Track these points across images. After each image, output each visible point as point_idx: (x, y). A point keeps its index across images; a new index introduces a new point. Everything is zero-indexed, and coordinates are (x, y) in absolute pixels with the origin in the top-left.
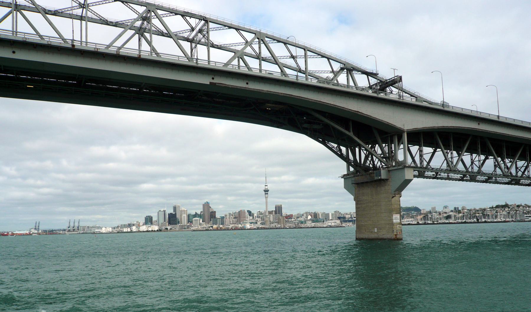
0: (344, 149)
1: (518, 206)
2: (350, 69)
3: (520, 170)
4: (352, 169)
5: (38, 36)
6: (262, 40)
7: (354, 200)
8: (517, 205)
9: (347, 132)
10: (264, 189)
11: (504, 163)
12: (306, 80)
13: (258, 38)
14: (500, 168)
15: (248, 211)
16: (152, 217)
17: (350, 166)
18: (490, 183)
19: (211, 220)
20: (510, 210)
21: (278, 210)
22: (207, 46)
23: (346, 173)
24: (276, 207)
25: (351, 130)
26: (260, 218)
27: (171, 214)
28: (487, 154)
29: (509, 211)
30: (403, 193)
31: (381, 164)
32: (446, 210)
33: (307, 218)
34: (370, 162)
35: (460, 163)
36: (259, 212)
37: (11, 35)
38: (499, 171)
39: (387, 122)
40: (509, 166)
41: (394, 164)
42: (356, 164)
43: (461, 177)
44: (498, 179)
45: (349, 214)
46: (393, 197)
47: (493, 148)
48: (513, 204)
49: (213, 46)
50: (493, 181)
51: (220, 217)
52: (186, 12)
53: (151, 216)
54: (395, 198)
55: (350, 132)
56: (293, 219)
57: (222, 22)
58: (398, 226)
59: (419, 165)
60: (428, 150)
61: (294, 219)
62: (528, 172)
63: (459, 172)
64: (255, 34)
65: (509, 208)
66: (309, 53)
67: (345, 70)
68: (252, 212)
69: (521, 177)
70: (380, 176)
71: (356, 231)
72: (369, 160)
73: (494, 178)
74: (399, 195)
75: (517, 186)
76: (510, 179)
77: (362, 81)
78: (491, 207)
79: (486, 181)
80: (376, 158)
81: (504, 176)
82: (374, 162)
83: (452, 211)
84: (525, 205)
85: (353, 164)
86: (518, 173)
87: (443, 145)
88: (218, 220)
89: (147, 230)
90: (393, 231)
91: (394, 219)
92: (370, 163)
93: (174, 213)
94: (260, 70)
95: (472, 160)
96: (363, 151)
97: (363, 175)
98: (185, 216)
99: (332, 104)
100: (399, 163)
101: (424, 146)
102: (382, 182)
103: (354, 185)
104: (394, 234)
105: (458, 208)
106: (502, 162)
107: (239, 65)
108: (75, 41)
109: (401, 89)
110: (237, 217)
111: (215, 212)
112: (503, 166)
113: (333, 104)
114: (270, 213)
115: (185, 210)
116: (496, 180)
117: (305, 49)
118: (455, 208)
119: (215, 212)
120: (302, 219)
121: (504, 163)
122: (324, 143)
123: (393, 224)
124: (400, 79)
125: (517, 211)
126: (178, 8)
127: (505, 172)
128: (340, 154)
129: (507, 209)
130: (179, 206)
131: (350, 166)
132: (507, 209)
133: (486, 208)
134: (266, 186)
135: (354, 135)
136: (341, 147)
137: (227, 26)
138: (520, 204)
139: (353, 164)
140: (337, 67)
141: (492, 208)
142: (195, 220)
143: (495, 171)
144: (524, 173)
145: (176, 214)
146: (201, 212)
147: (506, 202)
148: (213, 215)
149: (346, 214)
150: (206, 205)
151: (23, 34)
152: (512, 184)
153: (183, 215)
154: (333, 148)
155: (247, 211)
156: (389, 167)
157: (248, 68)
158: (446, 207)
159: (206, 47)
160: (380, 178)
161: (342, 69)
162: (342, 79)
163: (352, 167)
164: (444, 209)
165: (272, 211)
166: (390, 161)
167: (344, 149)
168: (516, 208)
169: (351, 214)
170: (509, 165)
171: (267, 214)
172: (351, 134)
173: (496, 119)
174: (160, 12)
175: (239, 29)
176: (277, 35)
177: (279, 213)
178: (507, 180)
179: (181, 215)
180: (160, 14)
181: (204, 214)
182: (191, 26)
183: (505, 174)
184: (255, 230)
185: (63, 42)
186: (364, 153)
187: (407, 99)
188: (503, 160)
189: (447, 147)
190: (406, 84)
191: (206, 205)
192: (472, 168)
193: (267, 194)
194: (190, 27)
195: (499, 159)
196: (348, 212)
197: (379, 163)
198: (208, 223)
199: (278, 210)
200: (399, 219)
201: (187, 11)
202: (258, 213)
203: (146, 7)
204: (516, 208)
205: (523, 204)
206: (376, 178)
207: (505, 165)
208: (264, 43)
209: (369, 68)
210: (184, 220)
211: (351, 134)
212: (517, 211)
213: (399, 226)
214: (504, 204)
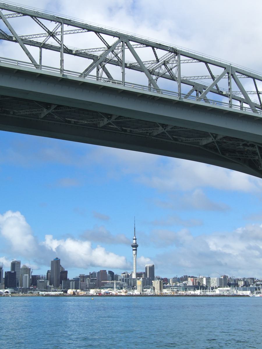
5: (33, 65)
12: (241, 109)
19: (61, 283)
22: (121, 66)
49: (69, 52)
52: (158, 44)
57: (193, 54)
64: (225, 68)
88: (71, 283)
93: (13, 272)
94: (241, 107)
107: (97, 76)
108: (65, 70)
110: (96, 279)
119: (66, 272)
126: (120, 31)
137: (197, 59)
145: (15, 273)
151: (17, 62)
155: (109, 271)
157: (35, 65)
159: (120, 67)
169: (245, 280)
174: (131, 43)
175: (35, 17)
180: (131, 45)
182: (107, 45)
185: (35, 68)
194: (106, 45)
201: (159, 43)
203: (118, 38)
208: (233, 77)
210: (26, 281)
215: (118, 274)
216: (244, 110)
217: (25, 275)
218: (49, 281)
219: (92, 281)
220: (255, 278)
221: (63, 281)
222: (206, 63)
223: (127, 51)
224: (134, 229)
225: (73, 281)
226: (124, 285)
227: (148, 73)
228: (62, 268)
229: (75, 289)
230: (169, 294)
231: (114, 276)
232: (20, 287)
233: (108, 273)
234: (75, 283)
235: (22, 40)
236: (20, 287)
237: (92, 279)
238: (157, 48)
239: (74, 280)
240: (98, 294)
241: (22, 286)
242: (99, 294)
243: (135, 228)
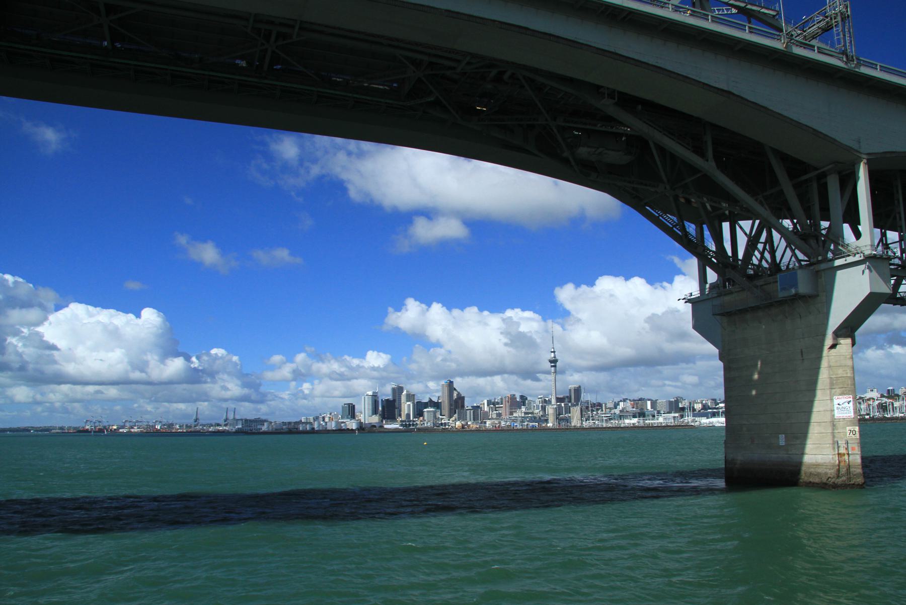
0: (691, 228)
7: (721, 359)
16: (354, 406)
17: (707, 268)
23: (696, 293)
27: (387, 400)
31: (794, 255)
34: (762, 254)
39: (815, 128)
53: (352, 404)
55: (707, 161)
58: (848, 428)
70: (795, 285)
71: (726, 443)
72: (759, 251)
80: (779, 236)
82: (773, 252)
85: (715, 261)
88: (468, 412)
89: (340, 428)
92: (762, 257)
97: (743, 290)
98: (410, 405)
99: (650, 63)
103: (718, 317)
110: (502, 407)
113: (657, 64)
128: (680, 233)
131: (707, 268)
135: (718, 168)
136: (687, 224)
139: (715, 261)
142: (428, 411)
154: (660, 218)
160: (793, 291)
163: (711, 268)
166: (819, 246)
167: (691, 228)
172: (709, 166)
184: (280, 436)
186: (746, 234)
197: (789, 253)
206: (782, 295)
211: (709, 166)
213: (851, 428)
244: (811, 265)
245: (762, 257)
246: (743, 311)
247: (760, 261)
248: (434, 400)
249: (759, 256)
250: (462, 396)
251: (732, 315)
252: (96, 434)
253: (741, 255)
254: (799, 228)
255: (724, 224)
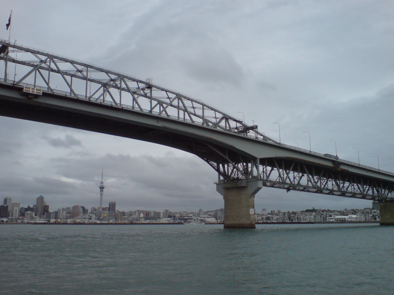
1: (323, 211)
2: (226, 118)
3: (322, 184)
4: (222, 178)
6: (180, 99)
8: (322, 210)
9: (224, 156)
10: (100, 186)
11: (313, 179)
13: (178, 98)
14: (311, 182)
15: (81, 207)
18: (305, 191)
19: (44, 214)
20: (317, 214)
21: (112, 206)
23: (218, 182)
24: (110, 204)
25: (227, 156)
26: (94, 214)
28: (303, 172)
29: (316, 215)
30: (256, 195)
32: (265, 213)
33: (140, 215)
34: (235, 174)
35: (288, 179)
36: (93, 208)
37: (46, 91)
38: (310, 184)
40: (316, 181)
41: (250, 177)
42: (224, 174)
43: (288, 187)
44: (309, 189)
45: (179, 214)
46: (250, 198)
47: (307, 169)
48: (319, 209)
50: (307, 190)
51: (54, 211)
54: (251, 198)
56: (126, 216)
59: (262, 179)
60: (269, 168)
61: (127, 216)
62: (327, 185)
63: (287, 184)
65: (316, 212)
66: (205, 107)
67: (224, 119)
68: (85, 208)
69: (323, 188)
73: (307, 189)
74: (253, 197)
75: (321, 194)
76: (317, 189)
77: (233, 124)
78: (302, 211)
79: (302, 190)
81: (314, 187)
83: (269, 214)
84: (328, 210)
86: (322, 186)
87: (278, 166)
88: (52, 215)
90: (250, 219)
91: (250, 211)
92: (235, 175)
93: (5, 206)
95: (294, 176)
96: (230, 167)
98: (17, 209)
100: (254, 177)
101: (267, 166)
102: (243, 188)
104: (250, 221)
105: (274, 211)
106: (312, 179)
109: (257, 133)
111: (48, 206)
112: (312, 181)
114: (104, 209)
115: (18, 203)
116: (308, 190)
117: (203, 105)
118: (272, 211)
119: (48, 206)
120: (135, 216)
121: (313, 179)
122: (207, 161)
123: (249, 215)
124: (256, 127)
125: (321, 215)
127: (314, 185)
129: (314, 213)
130: (10, 199)
132: (314, 213)
133: (298, 212)
134: (102, 184)
138: (324, 209)
140: (219, 116)
141: (303, 212)
143: (308, 184)
144: (325, 186)
146: (34, 206)
147: (313, 208)
148: (45, 209)
149: (176, 213)
150: (41, 199)
152: (318, 193)
153: (15, 208)
156: (248, 179)
158: (264, 210)
161: (223, 118)
162: (223, 123)
164: (262, 211)
165: (106, 208)
168: (321, 213)
169: (181, 213)
170: (316, 180)
171: (101, 210)
173: (309, 153)
176: (188, 96)
177: (112, 210)
178: (315, 190)
179: (13, 208)
181: (37, 208)
183: (314, 186)
187: (260, 138)
188: (313, 177)
189: (280, 167)
190: (259, 130)
191: (41, 199)
192: (294, 181)
193: (103, 191)
195: (311, 177)
196: (178, 212)
197: (241, 175)
198: (40, 217)
199: (112, 206)
200: (253, 211)
202: (92, 209)
203: (175, 95)
204: (321, 213)
205: (326, 210)
206: (240, 185)
207: (314, 180)
209: (238, 118)
212: (321, 215)
214: (312, 209)
215: (88, 209)
216: (7, 82)
217: (15, 208)
218: (34, 213)
219: (68, 213)
220: (188, 212)
221: (45, 213)
222: (166, 92)
223: (123, 83)
224: (102, 175)
225: (53, 213)
226: (92, 217)
227: (132, 93)
228: (45, 203)
229: (55, 219)
230: (127, 223)
231: (85, 210)
232: (11, 217)
233: (80, 208)
234: (55, 214)
235: (63, 72)
236: (11, 217)
237: (68, 212)
238: (140, 83)
239: (54, 212)
240: (74, 223)
241: (12, 216)
242: (75, 222)
243: (102, 175)
244: (246, 179)
245: (235, 175)
246: (230, 188)
247: (234, 176)
248: (31, 207)
249: (234, 175)
250: (47, 205)
251: (227, 189)
252: (147, 216)
253: (229, 175)
254: (356, 180)
255: (225, 165)
